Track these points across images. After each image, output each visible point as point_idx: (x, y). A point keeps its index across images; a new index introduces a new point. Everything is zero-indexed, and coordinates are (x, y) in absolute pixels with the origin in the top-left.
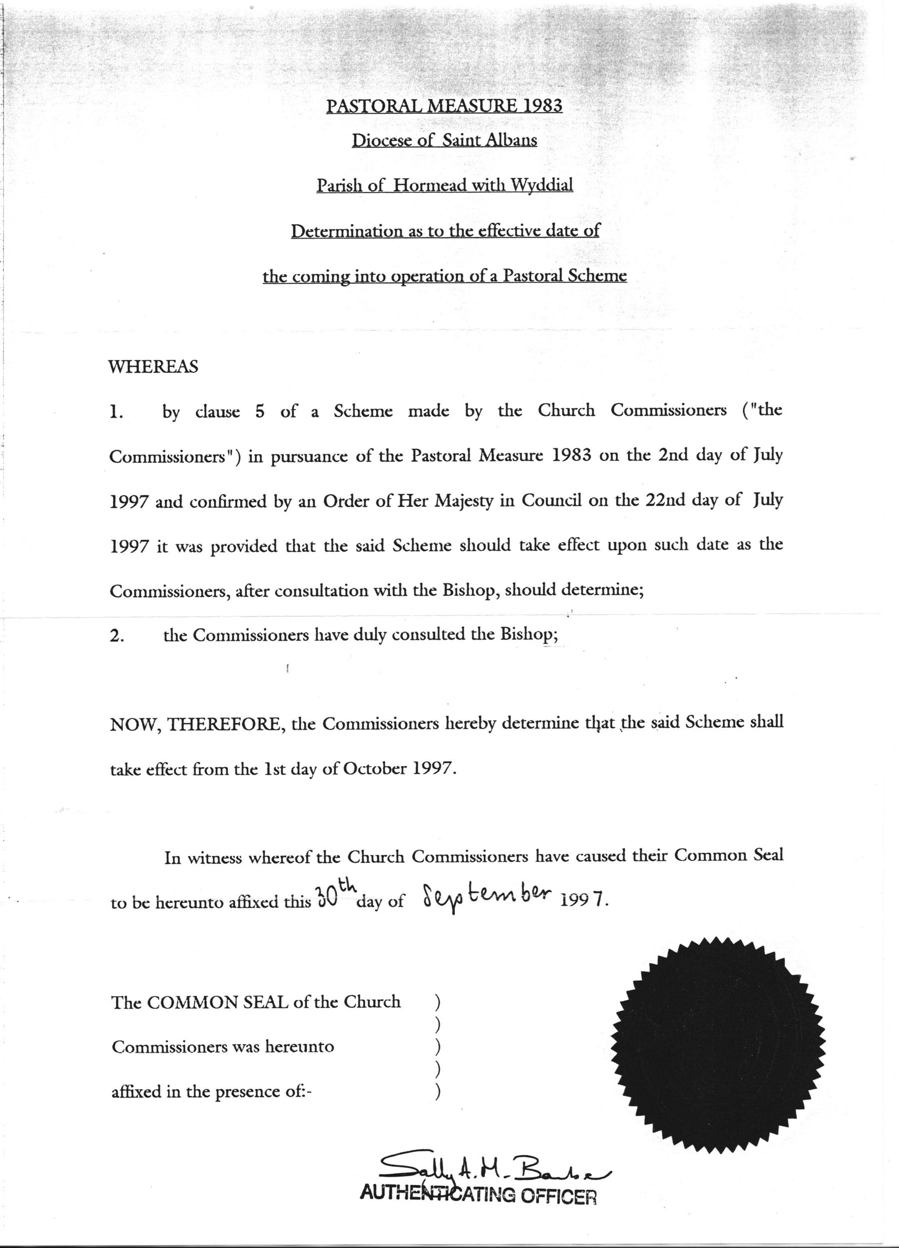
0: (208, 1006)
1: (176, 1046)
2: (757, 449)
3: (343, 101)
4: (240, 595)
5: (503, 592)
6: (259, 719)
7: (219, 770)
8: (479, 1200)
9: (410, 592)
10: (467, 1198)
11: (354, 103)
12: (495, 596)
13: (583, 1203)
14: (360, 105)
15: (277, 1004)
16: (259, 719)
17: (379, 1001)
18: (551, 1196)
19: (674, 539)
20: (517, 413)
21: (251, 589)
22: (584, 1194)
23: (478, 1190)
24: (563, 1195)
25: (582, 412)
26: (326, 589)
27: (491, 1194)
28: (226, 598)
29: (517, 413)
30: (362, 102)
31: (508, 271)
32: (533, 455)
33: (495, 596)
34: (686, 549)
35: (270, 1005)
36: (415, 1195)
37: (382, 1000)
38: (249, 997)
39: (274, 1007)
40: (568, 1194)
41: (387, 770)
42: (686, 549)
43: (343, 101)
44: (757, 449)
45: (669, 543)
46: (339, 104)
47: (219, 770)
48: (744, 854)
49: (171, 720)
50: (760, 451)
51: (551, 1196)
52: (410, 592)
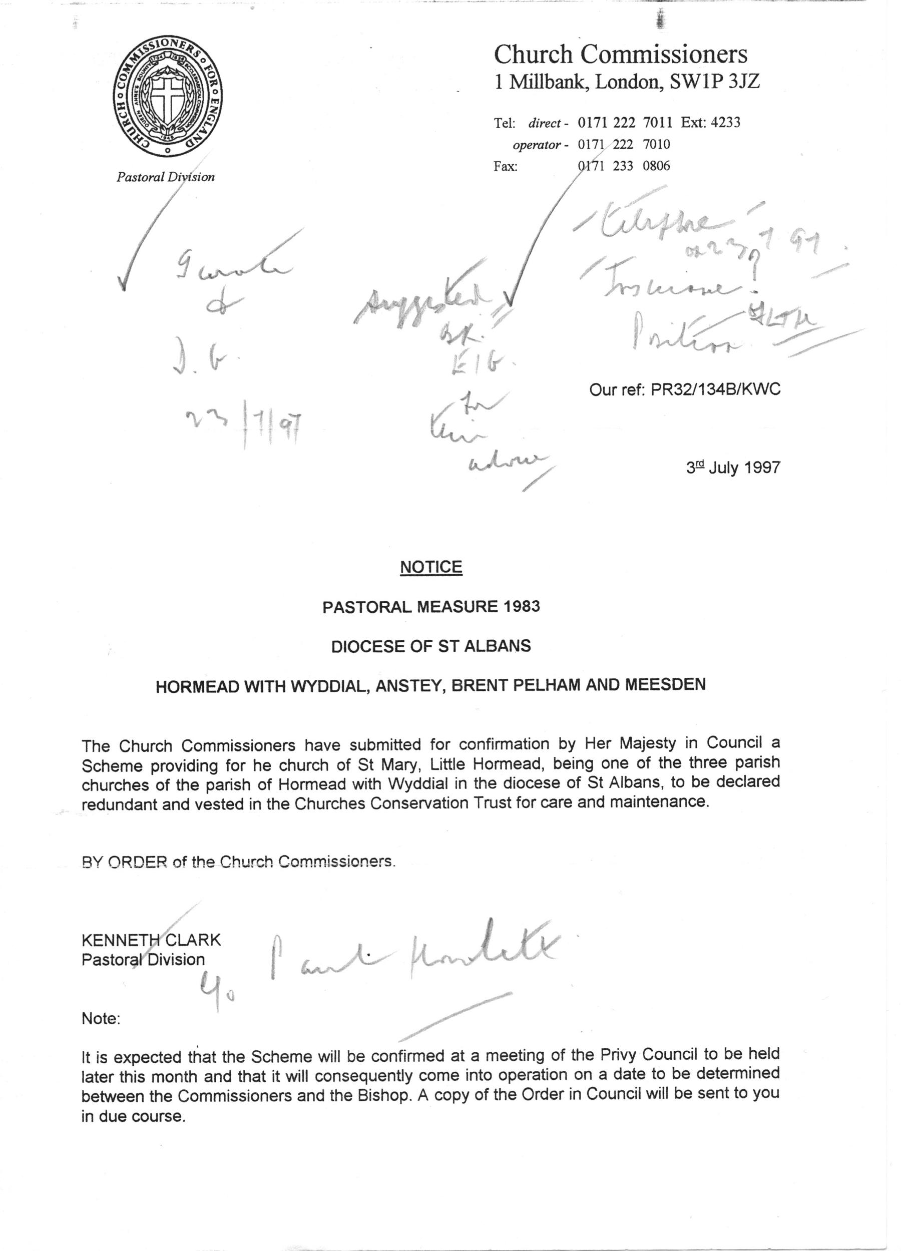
0: (687, 61)
1: (671, 52)
7: (619, 55)
8: (622, 787)
10: (561, 689)
13: (693, 689)
17: (542, 52)
18: (428, 646)
22: (155, 859)
23: (452, 338)
24: (375, 747)
25: (555, 57)
27: (410, 568)
31: (717, 76)
32: (545, 53)
34: (570, 62)
36: (643, 686)
37: (547, 51)
38: (675, 61)
40: (366, 644)
42: (570, 62)
47: (619, 55)
48: (656, 80)
51: (428, 646)
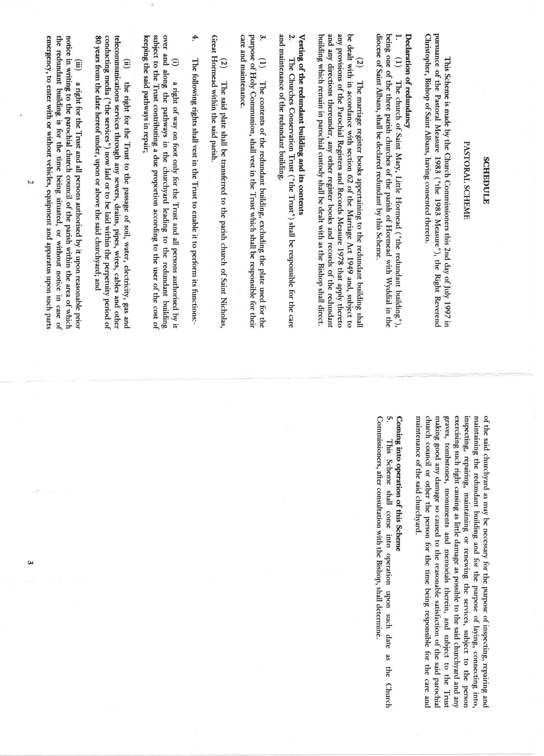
2: (450, 287)
3: (469, 148)
4: (378, 473)
5: (378, 586)
6: (469, 168)
9: (379, 546)
11: (468, 153)
12: (377, 583)
14: (467, 156)
15: (466, 178)
16: (469, 168)
19: (391, 622)
20: (388, 675)
21: (380, 478)
26: (380, 510)
28: (377, 467)
29: (388, 675)
30: (468, 157)
33: (377, 583)
35: (465, 175)
39: (465, 177)
41: (49, 195)
43: (469, 148)
44: (450, 287)
45: (389, 620)
46: (468, 146)
49: (294, 156)
50: (449, 288)
52: (379, 546)
